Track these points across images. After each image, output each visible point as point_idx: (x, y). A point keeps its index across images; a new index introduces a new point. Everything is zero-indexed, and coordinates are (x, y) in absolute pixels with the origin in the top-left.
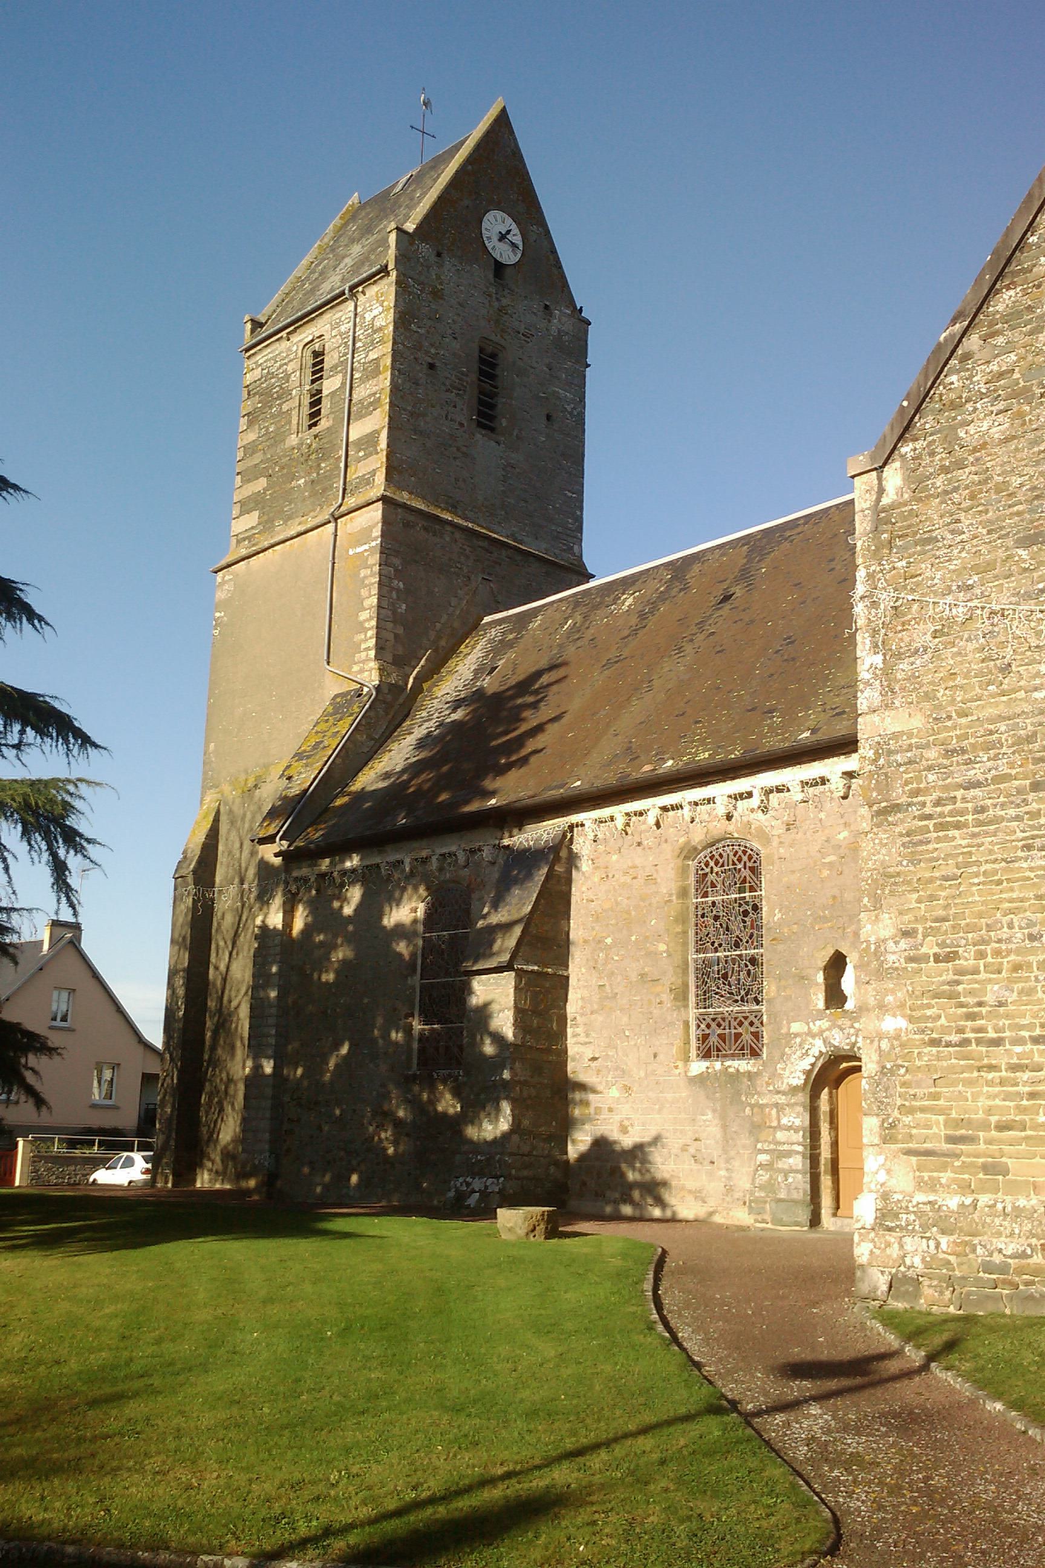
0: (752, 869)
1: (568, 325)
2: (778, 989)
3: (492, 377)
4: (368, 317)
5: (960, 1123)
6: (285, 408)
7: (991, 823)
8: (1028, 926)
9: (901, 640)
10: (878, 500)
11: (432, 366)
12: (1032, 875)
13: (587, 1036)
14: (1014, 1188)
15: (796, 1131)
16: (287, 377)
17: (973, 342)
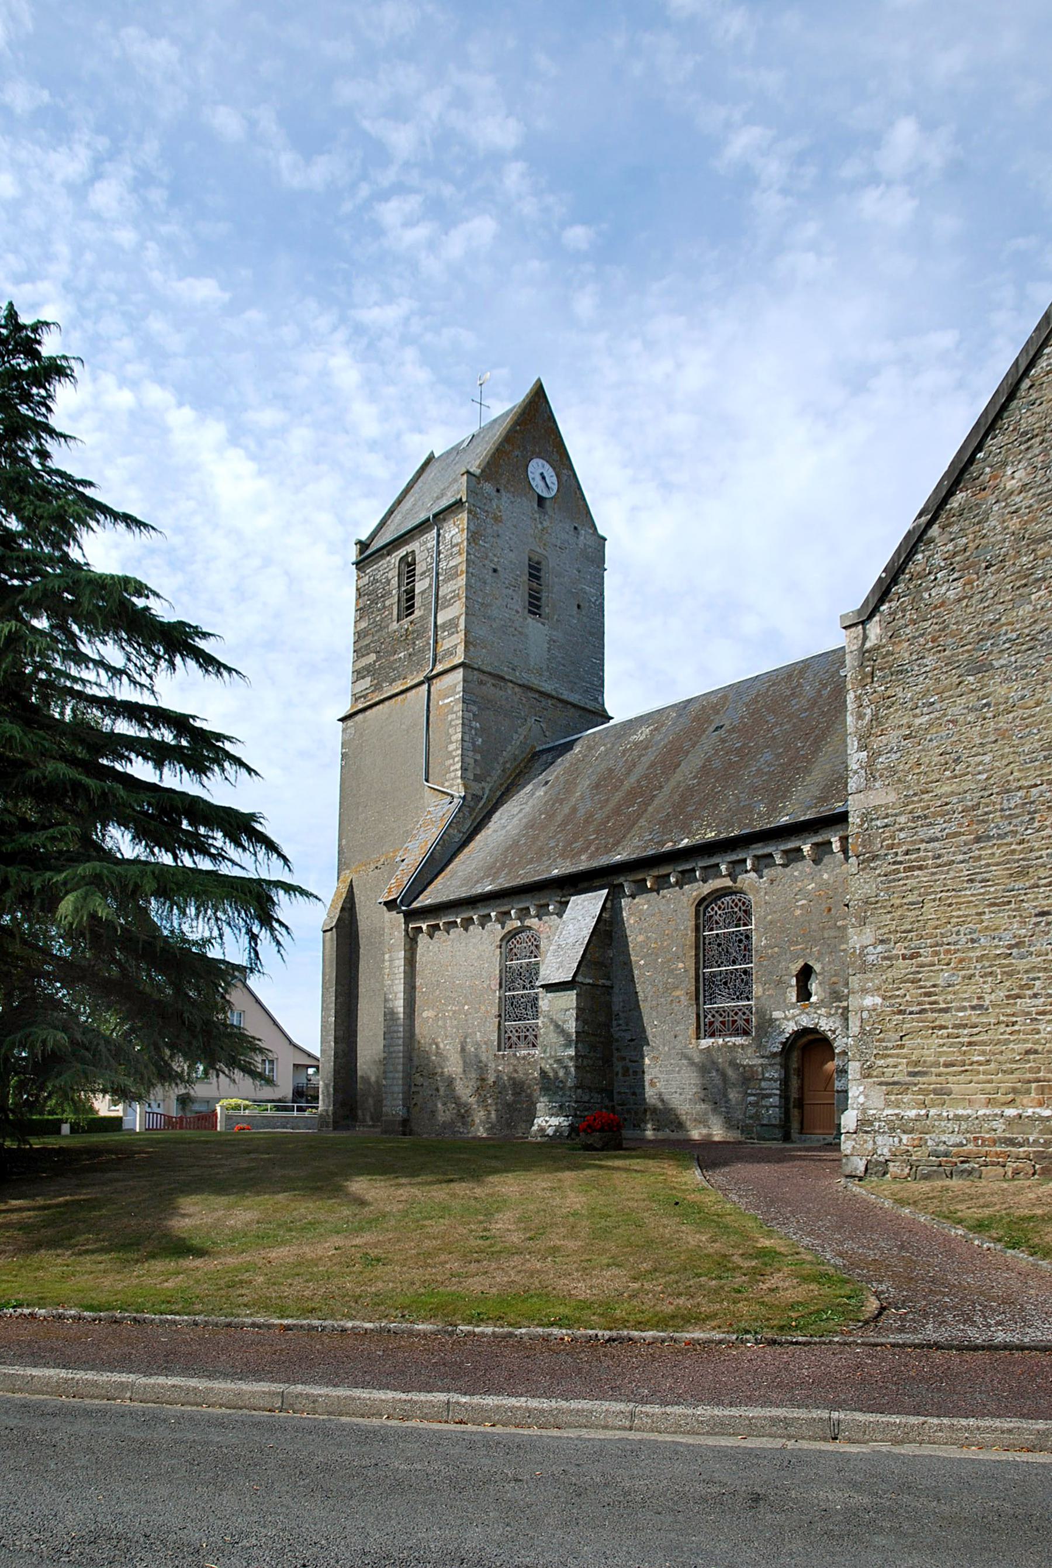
0: (745, 911)
1: (591, 541)
2: (764, 990)
3: (538, 578)
4: (448, 536)
5: (917, 1063)
6: (387, 603)
7: (945, 865)
8: (970, 933)
9: (881, 741)
10: (863, 644)
11: (495, 571)
12: (974, 899)
13: (627, 1025)
14: (956, 1103)
15: (775, 1081)
16: (388, 582)
17: (935, 531)
